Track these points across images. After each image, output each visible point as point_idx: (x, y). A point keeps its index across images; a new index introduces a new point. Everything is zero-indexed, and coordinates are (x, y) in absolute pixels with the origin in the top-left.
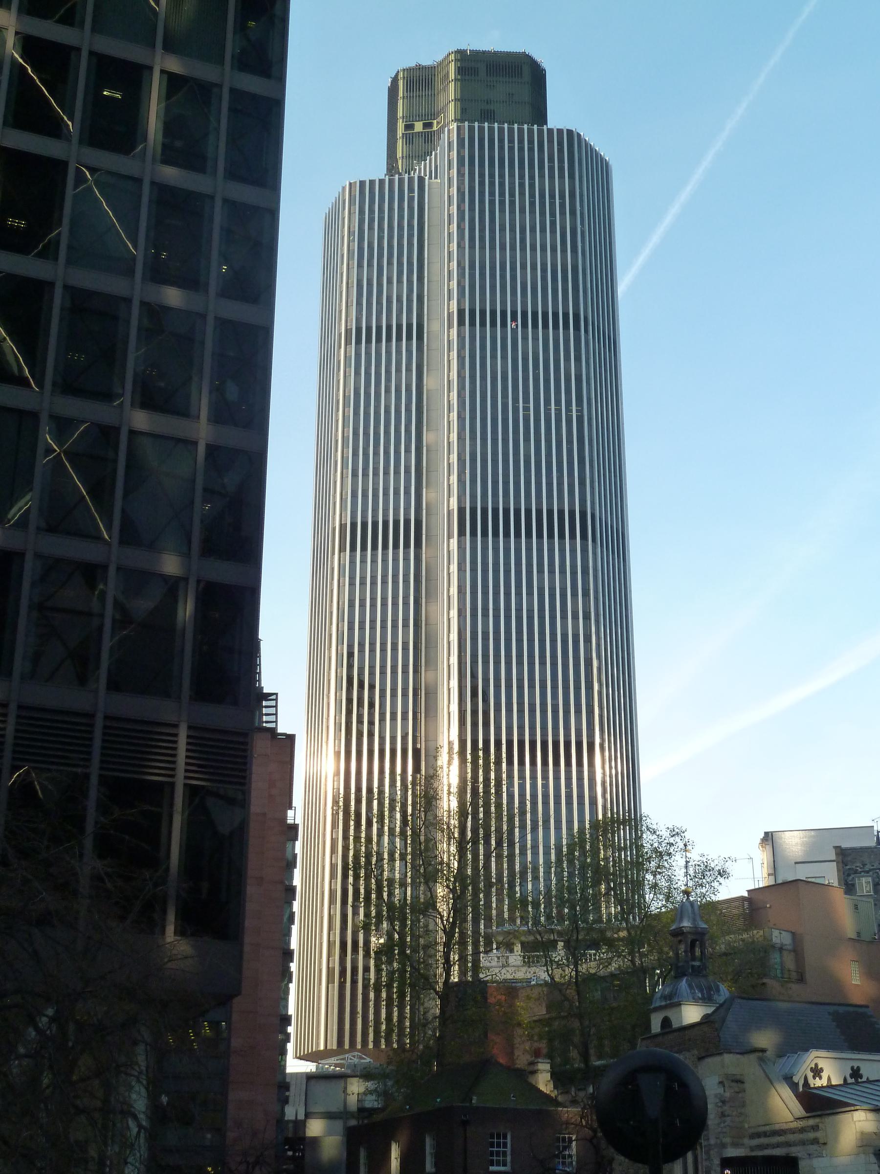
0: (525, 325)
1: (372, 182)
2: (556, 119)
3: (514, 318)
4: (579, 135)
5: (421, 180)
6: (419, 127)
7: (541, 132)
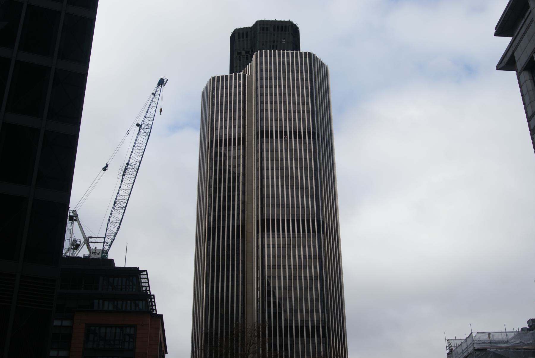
0: (291, 137)
1: (222, 77)
2: (304, 48)
3: (286, 135)
4: (314, 55)
5: (244, 75)
6: (243, 53)
7: (297, 54)
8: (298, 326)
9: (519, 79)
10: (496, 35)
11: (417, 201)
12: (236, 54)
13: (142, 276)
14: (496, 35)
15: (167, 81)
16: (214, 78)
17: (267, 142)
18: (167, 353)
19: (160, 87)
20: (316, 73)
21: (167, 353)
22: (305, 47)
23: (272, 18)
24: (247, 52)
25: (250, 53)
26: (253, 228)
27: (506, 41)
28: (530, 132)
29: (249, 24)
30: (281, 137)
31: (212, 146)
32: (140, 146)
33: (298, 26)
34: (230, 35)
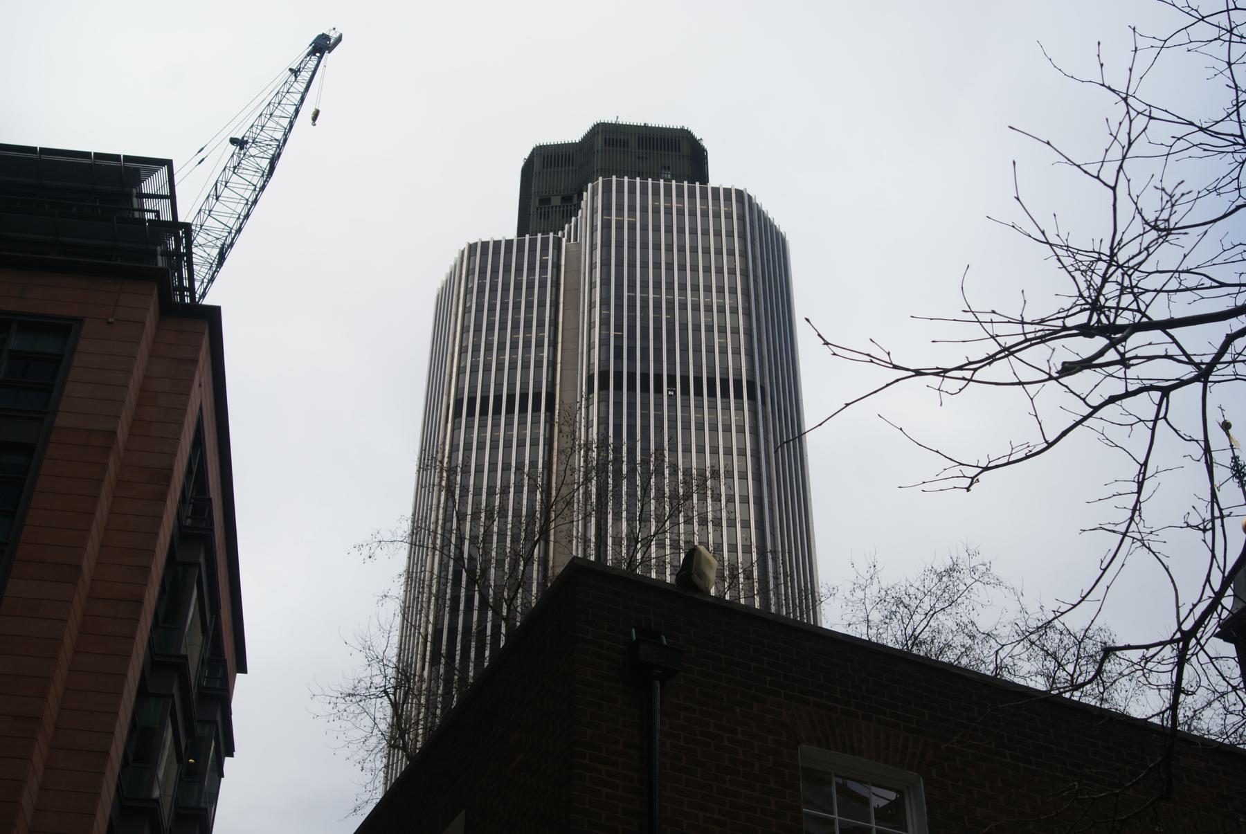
0: (685, 391)
1: (497, 244)
3: (672, 383)
4: (750, 197)
5: (558, 242)
6: (556, 201)
8: (741, 381)
12: (534, 203)
15: (339, 39)
16: (472, 247)
18: (244, 670)
19: (314, 59)
21: (244, 670)
22: (718, 176)
24: (567, 199)
25: (575, 201)
29: (573, 133)
30: (659, 389)
31: (458, 414)
32: (241, 187)
33: (705, 144)
34: (522, 164)
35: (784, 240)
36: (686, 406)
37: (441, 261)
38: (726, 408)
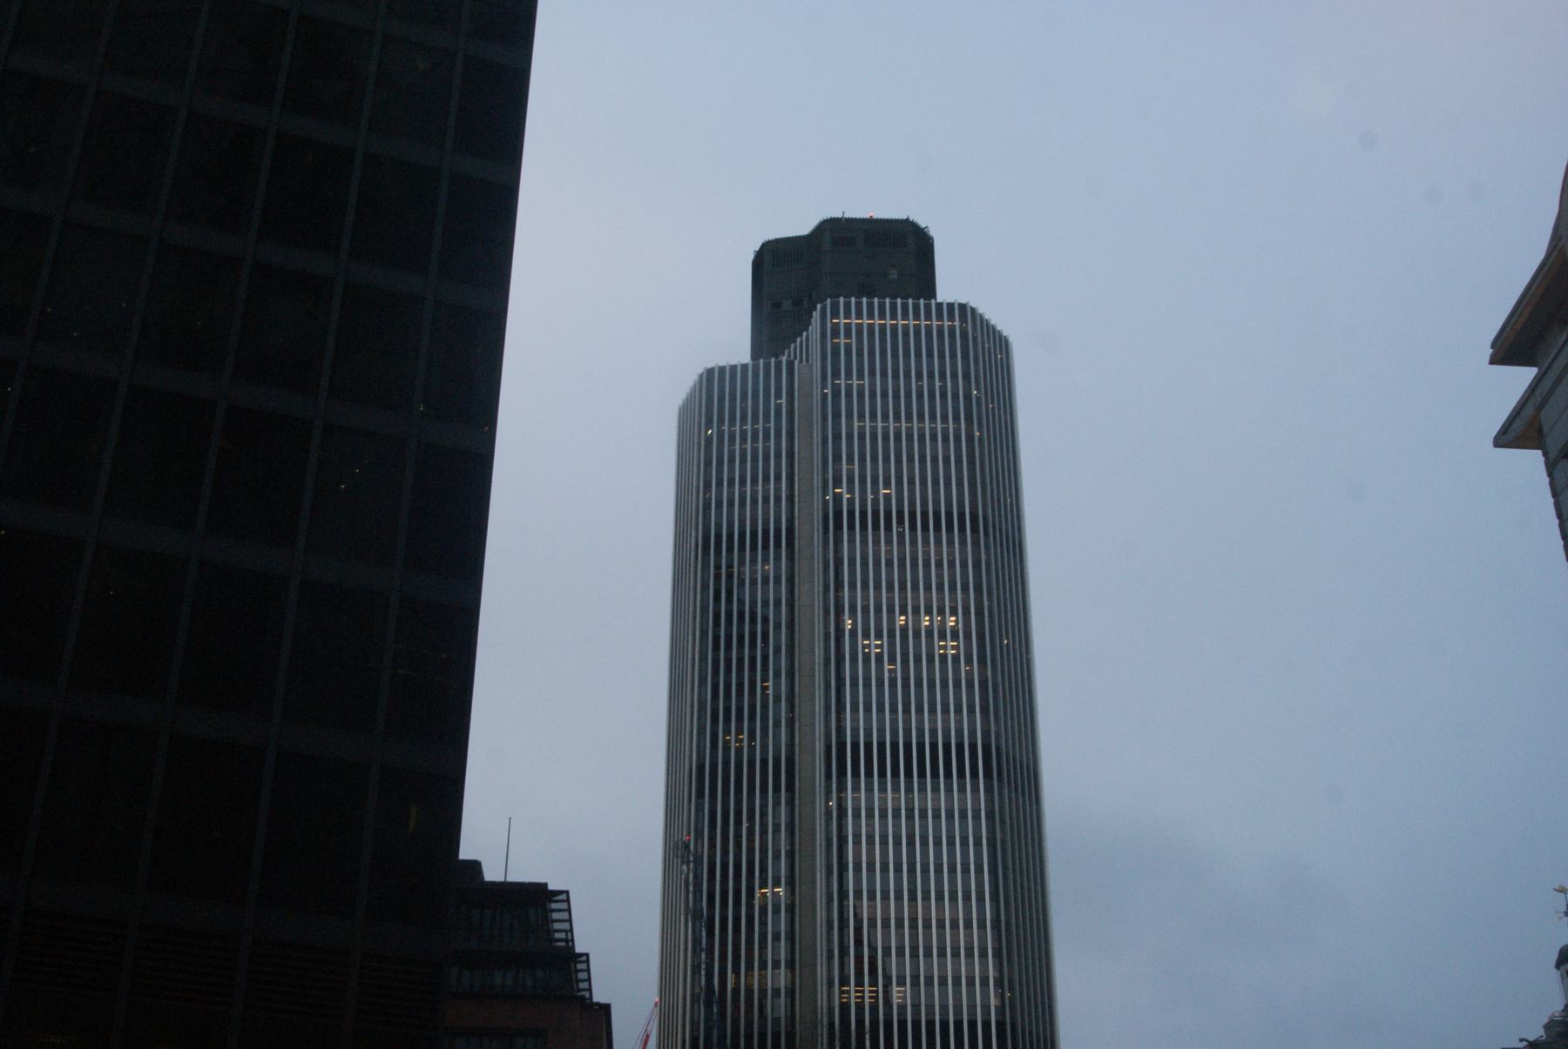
0: (913, 528)
1: (733, 368)
2: (946, 291)
4: (973, 310)
5: (790, 364)
6: (787, 305)
7: (928, 307)
9: (1550, 475)
10: (1493, 361)
11: (1205, 644)
13: (554, 906)
14: (1493, 361)
16: (710, 372)
17: (852, 541)
20: (977, 361)
23: (866, 215)
26: (814, 765)
27: (1521, 377)
28: (1561, 543)
29: (802, 226)
30: (888, 528)
33: (932, 232)
34: (752, 257)
35: (1007, 341)
36: (914, 542)
37: (676, 385)
38: (883, 789)
